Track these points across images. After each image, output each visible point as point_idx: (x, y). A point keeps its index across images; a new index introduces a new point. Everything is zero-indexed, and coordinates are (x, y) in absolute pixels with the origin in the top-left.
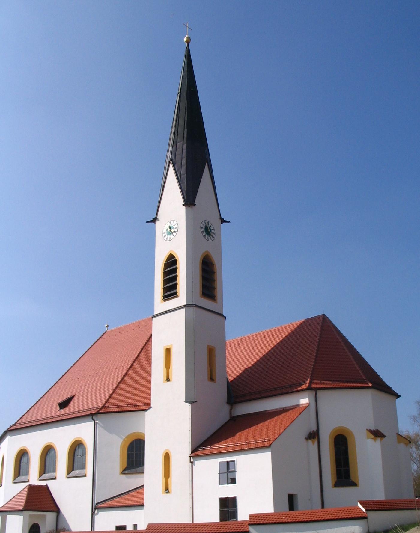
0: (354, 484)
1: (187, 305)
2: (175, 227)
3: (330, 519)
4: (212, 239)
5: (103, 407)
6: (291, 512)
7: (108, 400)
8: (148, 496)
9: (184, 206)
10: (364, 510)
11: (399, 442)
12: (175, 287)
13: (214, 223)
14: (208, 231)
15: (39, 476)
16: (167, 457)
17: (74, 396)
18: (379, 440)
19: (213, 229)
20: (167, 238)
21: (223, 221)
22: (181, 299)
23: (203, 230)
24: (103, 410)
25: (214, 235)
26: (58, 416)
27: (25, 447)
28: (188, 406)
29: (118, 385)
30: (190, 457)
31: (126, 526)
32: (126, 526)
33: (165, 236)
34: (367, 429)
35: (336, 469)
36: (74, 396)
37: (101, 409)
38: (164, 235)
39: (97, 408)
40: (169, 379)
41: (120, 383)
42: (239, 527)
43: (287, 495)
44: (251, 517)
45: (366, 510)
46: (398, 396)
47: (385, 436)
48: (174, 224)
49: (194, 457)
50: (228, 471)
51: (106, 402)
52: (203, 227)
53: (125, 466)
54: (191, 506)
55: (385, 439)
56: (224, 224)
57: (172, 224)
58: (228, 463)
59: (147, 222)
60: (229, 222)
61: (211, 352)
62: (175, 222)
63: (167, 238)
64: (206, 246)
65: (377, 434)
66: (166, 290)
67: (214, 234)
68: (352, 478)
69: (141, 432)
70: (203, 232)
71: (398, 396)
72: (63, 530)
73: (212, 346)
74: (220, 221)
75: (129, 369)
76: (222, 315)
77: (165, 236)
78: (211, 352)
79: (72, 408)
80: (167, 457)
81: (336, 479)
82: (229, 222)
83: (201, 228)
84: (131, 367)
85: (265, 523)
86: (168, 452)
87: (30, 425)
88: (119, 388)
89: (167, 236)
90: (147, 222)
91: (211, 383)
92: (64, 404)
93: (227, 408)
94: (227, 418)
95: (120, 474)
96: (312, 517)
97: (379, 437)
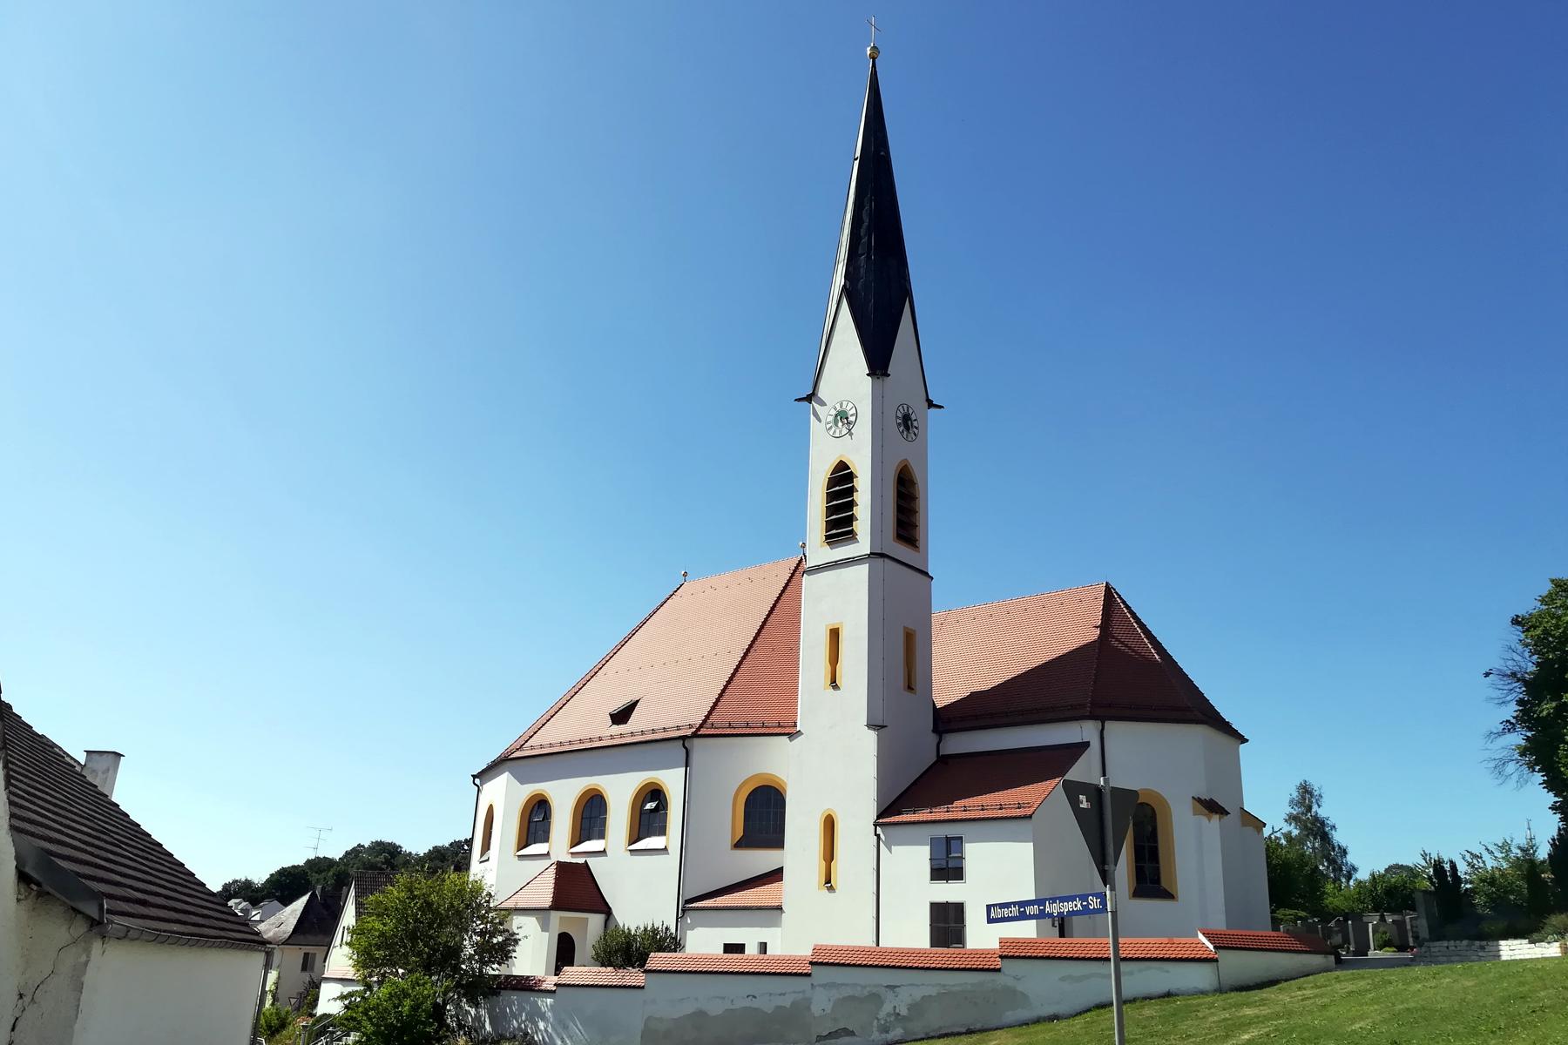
0: (1168, 895)
1: (871, 553)
2: (851, 412)
3: (1211, 958)
4: (914, 438)
5: (701, 726)
6: (1063, 940)
7: (710, 713)
8: (789, 892)
9: (869, 378)
10: (1211, 947)
11: (1244, 824)
12: (850, 520)
13: (918, 406)
14: (907, 422)
15: (629, 842)
16: (830, 824)
17: (638, 701)
18: (1216, 817)
19: (915, 420)
20: (835, 432)
21: (931, 404)
22: (863, 546)
23: (899, 421)
24: (703, 731)
25: (916, 431)
26: (612, 737)
27: (543, 790)
28: (872, 736)
29: (726, 687)
30: (876, 825)
31: (744, 945)
32: (744, 945)
33: (831, 428)
34: (1193, 797)
35: (1136, 867)
36: (638, 701)
37: (698, 729)
38: (828, 426)
39: (691, 726)
40: (835, 682)
41: (729, 682)
42: (969, 959)
43: (929, 904)
44: (1003, 944)
45: (1214, 947)
46: (1244, 740)
47: (1227, 813)
48: (848, 408)
49: (881, 825)
50: (948, 857)
51: (707, 717)
52: (900, 415)
53: (740, 833)
54: (875, 915)
55: (1226, 818)
56: (823, 392)
57: (844, 407)
58: (948, 840)
59: (796, 400)
60: (943, 407)
61: (909, 637)
62: (850, 405)
63: (835, 432)
64: (902, 450)
65: (1211, 807)
66: (830, 525)
67: (916, 428)
68: (1164, 884)
69: (769, 772)
70: (899, 425)
71: (1244, 740)
72: (668, 947)
73: (911, 630)
74: (926, 404)
75: (744, 658)
76: (926, 574)
77: (831, 428)
78: (909, 637)
79: (636, 722)
80: (830, 824)
81: (1135, 885)
82: (943, 407)
83: (897, 417)
84: (746, 654)
85: (1162, 958)
86: (830, 813)
87: (588, 745)
88: (726, 695)
89: (833, 429)
90: (796, 400)
91: (907, 694)
92: (621, 717)
93: (932, 739)
94: (935, 759)
95: (732, 849)
96: (1103, 952)
97: (1217, 813)
